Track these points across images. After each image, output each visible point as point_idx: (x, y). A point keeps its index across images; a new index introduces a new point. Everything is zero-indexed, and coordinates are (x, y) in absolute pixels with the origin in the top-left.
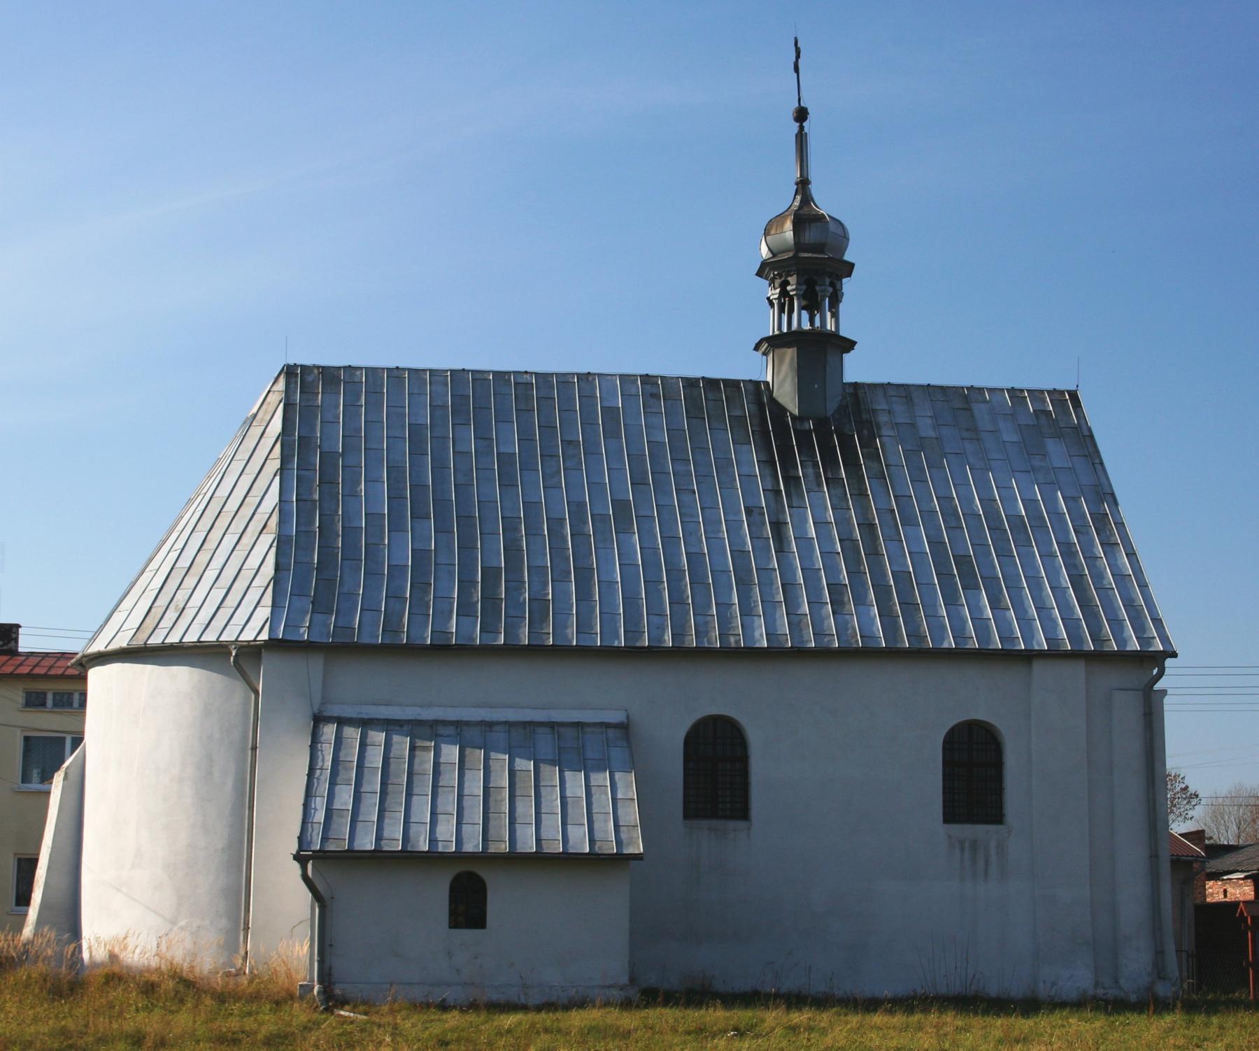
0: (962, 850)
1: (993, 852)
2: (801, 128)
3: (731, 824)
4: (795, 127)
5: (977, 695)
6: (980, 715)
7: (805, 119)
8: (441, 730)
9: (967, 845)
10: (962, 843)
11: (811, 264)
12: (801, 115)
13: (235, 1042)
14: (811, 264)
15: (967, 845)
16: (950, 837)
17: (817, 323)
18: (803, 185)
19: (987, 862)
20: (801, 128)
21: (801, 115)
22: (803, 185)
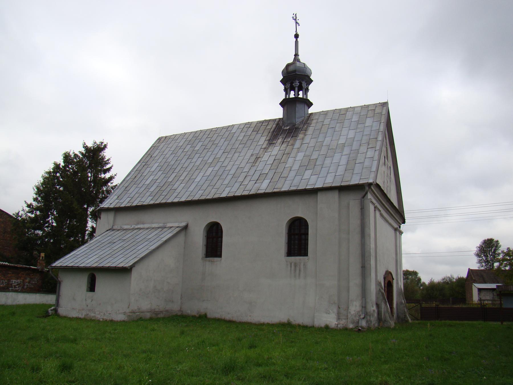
0: (291, 267)
1: (302, 267)
2: (297, 40)
3: (216, 259)
4: (295, 39)
5: (298, 209)
6: (299, 215)
7: (298, 37)
8: (364, 299)
9: (293, 264)
10: (291, 264)
11: (296, 78)
12: (297, 36)
13: (74, 382)
14: (296, 78)
15: (293, 264)
16: (287, 262)
17: (301, 96)
18: (296, 55)
19: (300, 270)
20: (297, 40)
21: (297, 36)
22: (296, 55)
